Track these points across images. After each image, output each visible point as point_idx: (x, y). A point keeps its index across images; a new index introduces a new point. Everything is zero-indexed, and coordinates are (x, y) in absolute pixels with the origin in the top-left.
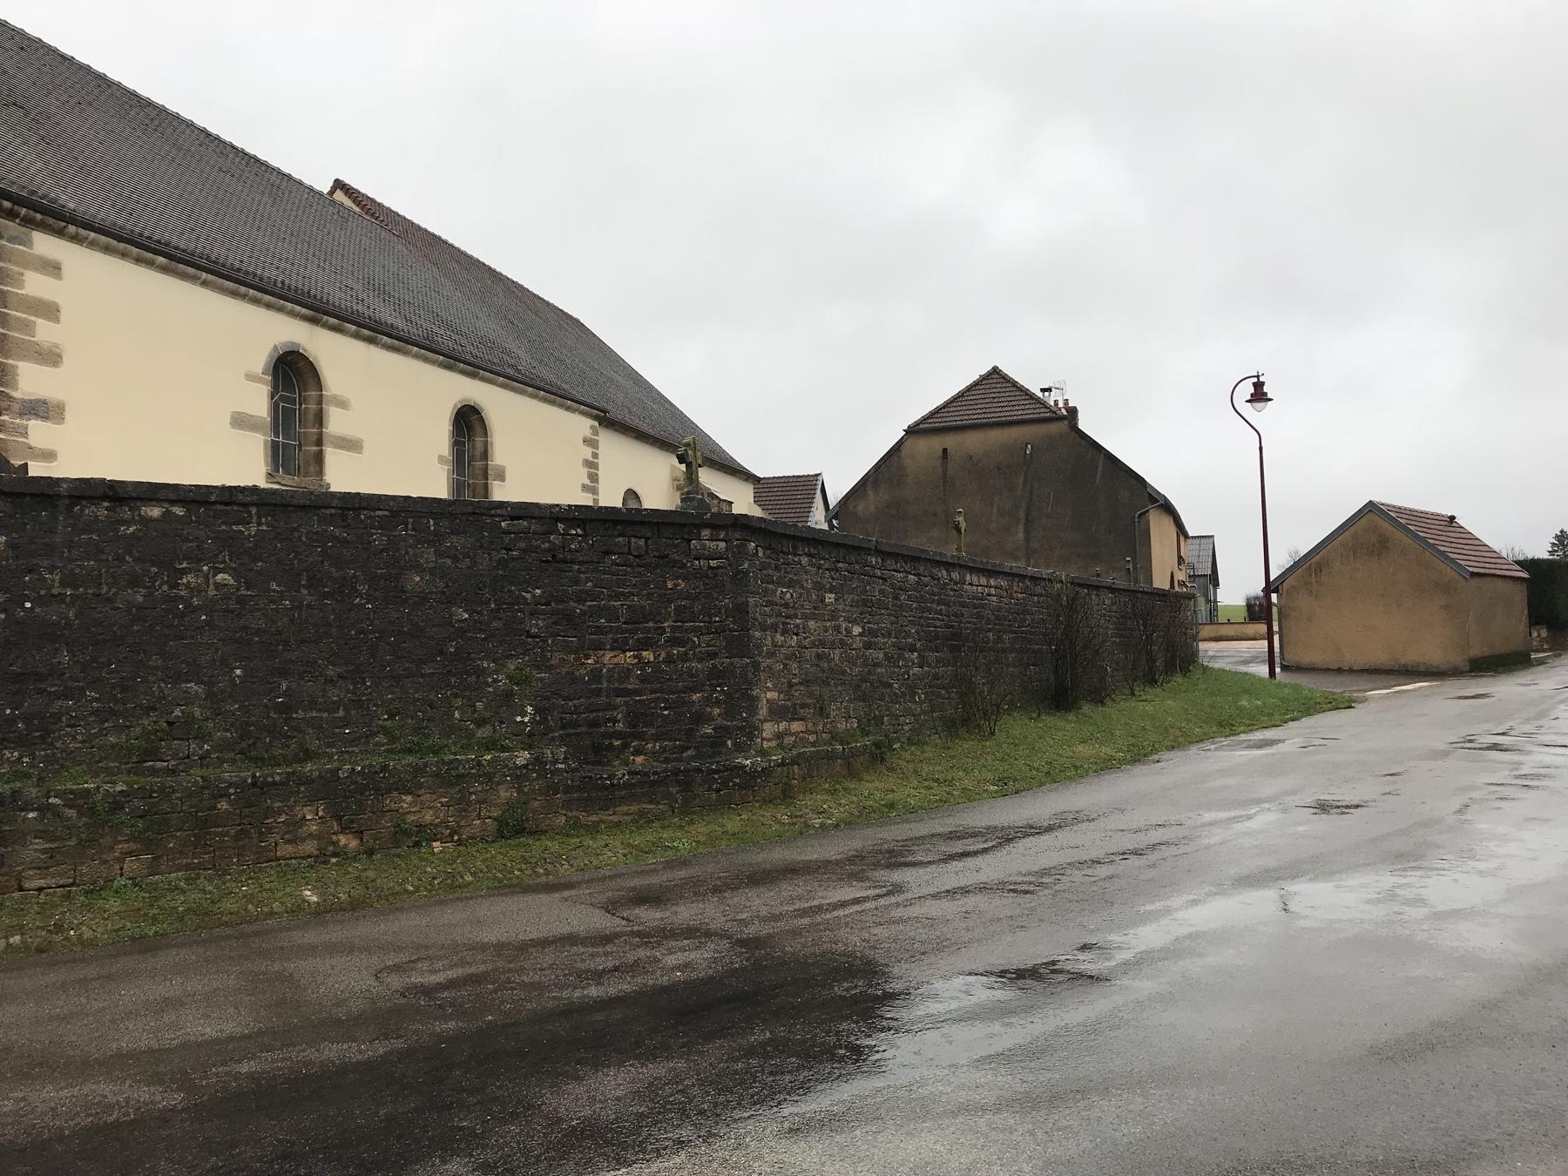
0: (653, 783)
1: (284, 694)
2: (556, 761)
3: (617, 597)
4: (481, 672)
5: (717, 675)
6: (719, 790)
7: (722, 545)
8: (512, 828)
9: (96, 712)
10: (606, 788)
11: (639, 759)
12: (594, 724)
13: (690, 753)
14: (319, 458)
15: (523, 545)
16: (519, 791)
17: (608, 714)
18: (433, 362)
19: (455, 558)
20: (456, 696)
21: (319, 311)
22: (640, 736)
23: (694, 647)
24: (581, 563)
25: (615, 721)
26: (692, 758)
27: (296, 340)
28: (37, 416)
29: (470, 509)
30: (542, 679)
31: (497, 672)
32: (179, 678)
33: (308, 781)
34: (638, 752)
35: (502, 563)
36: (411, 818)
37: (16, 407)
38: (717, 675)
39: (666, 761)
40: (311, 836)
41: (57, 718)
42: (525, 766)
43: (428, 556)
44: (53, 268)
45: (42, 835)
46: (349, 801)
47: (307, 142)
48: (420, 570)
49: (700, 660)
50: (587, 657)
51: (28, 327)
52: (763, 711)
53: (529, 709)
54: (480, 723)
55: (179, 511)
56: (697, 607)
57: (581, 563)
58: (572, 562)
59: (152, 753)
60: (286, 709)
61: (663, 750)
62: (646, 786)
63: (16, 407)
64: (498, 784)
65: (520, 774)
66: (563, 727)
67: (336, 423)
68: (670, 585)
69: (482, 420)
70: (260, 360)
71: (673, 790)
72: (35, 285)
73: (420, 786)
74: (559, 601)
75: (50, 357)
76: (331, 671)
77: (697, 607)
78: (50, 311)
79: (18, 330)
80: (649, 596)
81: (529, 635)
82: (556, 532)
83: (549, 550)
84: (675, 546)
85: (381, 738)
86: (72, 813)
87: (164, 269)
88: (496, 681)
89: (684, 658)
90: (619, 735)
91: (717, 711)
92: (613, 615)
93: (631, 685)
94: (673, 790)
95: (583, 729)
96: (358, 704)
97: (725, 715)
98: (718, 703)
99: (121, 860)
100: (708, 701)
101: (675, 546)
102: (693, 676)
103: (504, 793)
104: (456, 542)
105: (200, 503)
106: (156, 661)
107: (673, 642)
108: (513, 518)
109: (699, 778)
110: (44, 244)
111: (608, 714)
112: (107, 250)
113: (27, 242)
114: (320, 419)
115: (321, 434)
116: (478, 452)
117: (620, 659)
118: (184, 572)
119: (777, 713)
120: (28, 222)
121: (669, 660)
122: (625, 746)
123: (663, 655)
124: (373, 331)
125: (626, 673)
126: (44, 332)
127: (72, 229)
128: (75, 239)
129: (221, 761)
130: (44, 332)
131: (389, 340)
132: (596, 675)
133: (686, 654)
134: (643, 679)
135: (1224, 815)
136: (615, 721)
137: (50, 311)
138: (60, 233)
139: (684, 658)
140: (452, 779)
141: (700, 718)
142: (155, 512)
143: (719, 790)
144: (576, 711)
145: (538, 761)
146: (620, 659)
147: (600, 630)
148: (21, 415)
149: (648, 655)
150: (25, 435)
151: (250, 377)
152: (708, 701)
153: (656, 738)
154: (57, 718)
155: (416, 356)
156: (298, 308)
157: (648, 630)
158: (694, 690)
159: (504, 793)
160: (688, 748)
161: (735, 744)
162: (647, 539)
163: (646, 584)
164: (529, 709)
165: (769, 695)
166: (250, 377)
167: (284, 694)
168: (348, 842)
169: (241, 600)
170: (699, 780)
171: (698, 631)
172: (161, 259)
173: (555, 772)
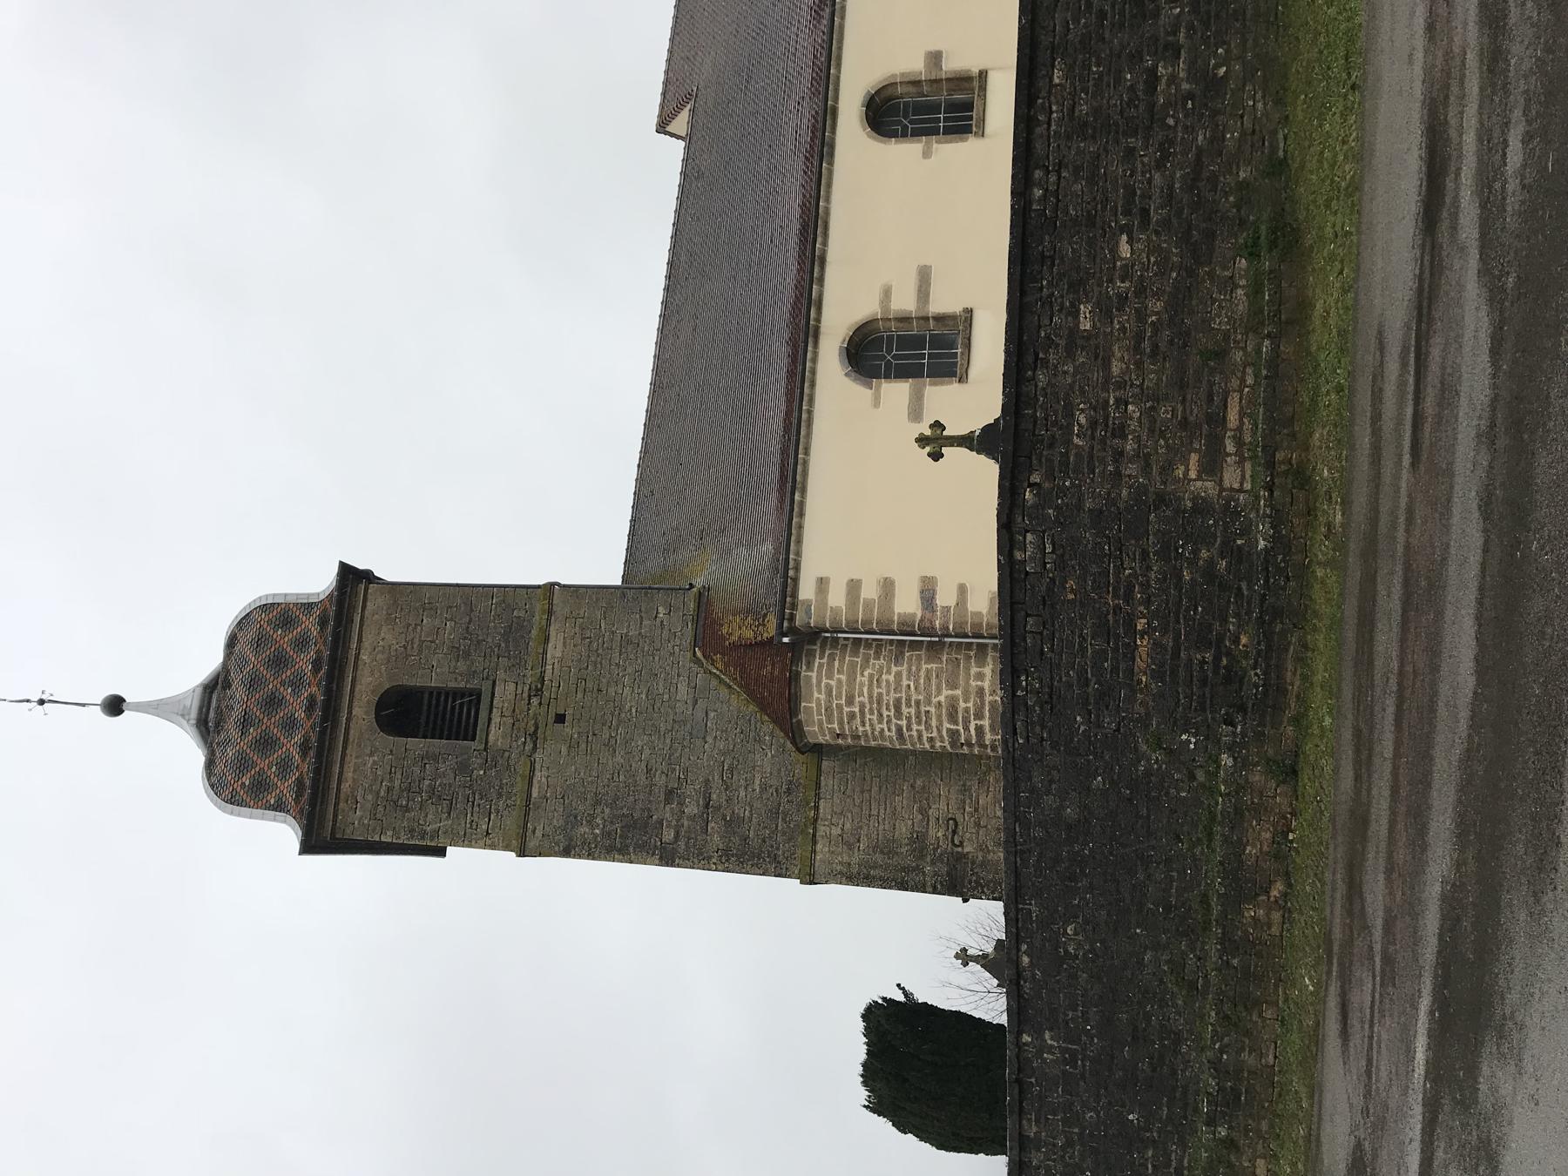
0: (1269, 647)
1: (1157, 906)
2: (1234, 733)
3: (1083, 650)
4: (1148, 773)
5: (1167, 551)
6: (1288, 578)
7: (1029, 537)
8: (1289, 772)
9: (1160, 1007)
10: (1265, 693)
11: (1244, 640)
12: (1204, 682)
13: (1244, 585)
14: (940, 319)
15: (1038, 729)
16: (1255, 765)
17: (1196, 667)
18: (830, 172)
19: (1051, 782)
20: (1167, 794)
21: (804, 332)
22: (1220, 639)
23: (1134, 575)
24: (1052, 678)
25: (1203, 662)
26: (1250, 588)
27: (837, 352)
28: (933, 598)
29: (1010, 767)
30: (1158, 724)
31: (1149, 760)
32: (1141, 963)
33: (1224, 914)
34: (1236, 641)
35: (1055, 746)
36: (1265, 848)
37: (928, 615)
38: (1167, 551)
39: (1249, 613)
40: (1268, 915)
41: (1162, 1026)
42: (1235, 759)
43: (1049, 800)
44: (822, 583)
45: (1239, 1052)
46: (1243, 885)
47: (644, 181)
48: (1062, 807)
49: (1149, 568)
50: (1139, 682)
51: (868, 604)
52: (1208, 487)
53: (1184, 737)
54: (1192, 777)
55: (1024, 947)
56: (1094, 569)
57: (1052, 678)
58: (1051, 687)
59: (1192, 986)
60: (1168, 908)
61: (1237, 615)
62: (1270, 651)
63: (928, 615)
64: (1247, 781)
65: (1242, 764)
66: (1204, 710)
67: (904, 302)
68: (1071, 596)
69: (878, 92)
70: (858, 392)
71: (1278, 628)
72: (837, 598)
73: (1240, 839)
74: (1087, 702)
75: (888, 586)
76: (1141, 876)
77: (1094, 569)
78: (854, 587)
79: (872, 611)
80: (1083, 618)
81: (1118, 730)
82: (1024, 698)
83: (1042, 708)
84: (1033, 587)
85: (1197, 851)
86: (1226, 1040)
87: (804, 491)
88: (1157, 761)
89: (1146, 586)
90: (1217, 659)
91: (1204, 554)
92: (1101, 655)
93: (1169, 642)
94: (1278, 628)
95: (1207, 690)
96: (1168, 861)
97: (1209, 546)
98: (1195, 552)
99: (1264, 1019)
100: (1192, 563)
101: (1033, 587)
102: (1165, 579)
103: (1257, 778)
104: (1038, 779)
105: (1018, 934)
106: (1128, 973)
107: (1128, 597)
108: (1015, 733)
109: (1270, 600)
110: (806, 591)
111: (1196, 667)
112: (799, 541)
113: (808, 604)
114: (904, 319)
115: (918, 318)
116: (911, 89)
117: (1143, 651)
118: (1066, 951)
119: (1212, 467)
120: (794, 606)
121: (1147, 602)
122: (1229, 654)
123: (1141, 608)
124: (811, 261)
125: (1156, 645)
126: (869, 592)
127: (791, 573)
128: (797, 569)
129: (1202, 949)
130: (869, 592)
131: (819, 239)
132: (1157, 675)
133: (1141, 585)
134: (1164, 632)
135: (1378, 968)
136: (1203, 662)
137: (854, 587)
138: (796, 580)
139: (1146, 586)
140: (1237, 816)
141: (1209, 572)
142: (1026, 960)
143: (1288, 578)
144: (1189, 697)
145: (1230, 749)
146: (1143, 651)
147: (1115, 669)
148: (934, 611)
149: (1141, 624)
150: (948, 609)
151: (876, 402)
152: (1192, 563)
153: (1225, 621)
154: (1162, 1026)
155: (828, 200)
156: (809, 355)
157: (1116, 621)
158: (1180, 577)
159: (1257, 778)
160: (1239, 589)
161: (1241, 536)
162: (1028, 615)
163: (1071, 621)
164: (1184, 737)
165: (1193, 474)
166: (876, 402)
167: (1157, 906)
168: (1277, 890)
169: (1086, 922)
170: (1273, 600)
171: (1120, 568)
172: (797, 497)
173: (1243, 734)
